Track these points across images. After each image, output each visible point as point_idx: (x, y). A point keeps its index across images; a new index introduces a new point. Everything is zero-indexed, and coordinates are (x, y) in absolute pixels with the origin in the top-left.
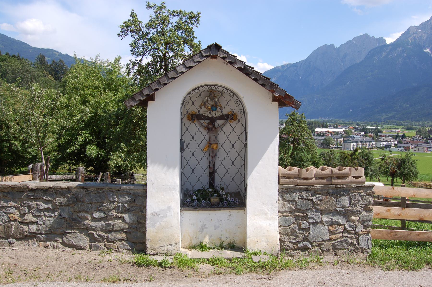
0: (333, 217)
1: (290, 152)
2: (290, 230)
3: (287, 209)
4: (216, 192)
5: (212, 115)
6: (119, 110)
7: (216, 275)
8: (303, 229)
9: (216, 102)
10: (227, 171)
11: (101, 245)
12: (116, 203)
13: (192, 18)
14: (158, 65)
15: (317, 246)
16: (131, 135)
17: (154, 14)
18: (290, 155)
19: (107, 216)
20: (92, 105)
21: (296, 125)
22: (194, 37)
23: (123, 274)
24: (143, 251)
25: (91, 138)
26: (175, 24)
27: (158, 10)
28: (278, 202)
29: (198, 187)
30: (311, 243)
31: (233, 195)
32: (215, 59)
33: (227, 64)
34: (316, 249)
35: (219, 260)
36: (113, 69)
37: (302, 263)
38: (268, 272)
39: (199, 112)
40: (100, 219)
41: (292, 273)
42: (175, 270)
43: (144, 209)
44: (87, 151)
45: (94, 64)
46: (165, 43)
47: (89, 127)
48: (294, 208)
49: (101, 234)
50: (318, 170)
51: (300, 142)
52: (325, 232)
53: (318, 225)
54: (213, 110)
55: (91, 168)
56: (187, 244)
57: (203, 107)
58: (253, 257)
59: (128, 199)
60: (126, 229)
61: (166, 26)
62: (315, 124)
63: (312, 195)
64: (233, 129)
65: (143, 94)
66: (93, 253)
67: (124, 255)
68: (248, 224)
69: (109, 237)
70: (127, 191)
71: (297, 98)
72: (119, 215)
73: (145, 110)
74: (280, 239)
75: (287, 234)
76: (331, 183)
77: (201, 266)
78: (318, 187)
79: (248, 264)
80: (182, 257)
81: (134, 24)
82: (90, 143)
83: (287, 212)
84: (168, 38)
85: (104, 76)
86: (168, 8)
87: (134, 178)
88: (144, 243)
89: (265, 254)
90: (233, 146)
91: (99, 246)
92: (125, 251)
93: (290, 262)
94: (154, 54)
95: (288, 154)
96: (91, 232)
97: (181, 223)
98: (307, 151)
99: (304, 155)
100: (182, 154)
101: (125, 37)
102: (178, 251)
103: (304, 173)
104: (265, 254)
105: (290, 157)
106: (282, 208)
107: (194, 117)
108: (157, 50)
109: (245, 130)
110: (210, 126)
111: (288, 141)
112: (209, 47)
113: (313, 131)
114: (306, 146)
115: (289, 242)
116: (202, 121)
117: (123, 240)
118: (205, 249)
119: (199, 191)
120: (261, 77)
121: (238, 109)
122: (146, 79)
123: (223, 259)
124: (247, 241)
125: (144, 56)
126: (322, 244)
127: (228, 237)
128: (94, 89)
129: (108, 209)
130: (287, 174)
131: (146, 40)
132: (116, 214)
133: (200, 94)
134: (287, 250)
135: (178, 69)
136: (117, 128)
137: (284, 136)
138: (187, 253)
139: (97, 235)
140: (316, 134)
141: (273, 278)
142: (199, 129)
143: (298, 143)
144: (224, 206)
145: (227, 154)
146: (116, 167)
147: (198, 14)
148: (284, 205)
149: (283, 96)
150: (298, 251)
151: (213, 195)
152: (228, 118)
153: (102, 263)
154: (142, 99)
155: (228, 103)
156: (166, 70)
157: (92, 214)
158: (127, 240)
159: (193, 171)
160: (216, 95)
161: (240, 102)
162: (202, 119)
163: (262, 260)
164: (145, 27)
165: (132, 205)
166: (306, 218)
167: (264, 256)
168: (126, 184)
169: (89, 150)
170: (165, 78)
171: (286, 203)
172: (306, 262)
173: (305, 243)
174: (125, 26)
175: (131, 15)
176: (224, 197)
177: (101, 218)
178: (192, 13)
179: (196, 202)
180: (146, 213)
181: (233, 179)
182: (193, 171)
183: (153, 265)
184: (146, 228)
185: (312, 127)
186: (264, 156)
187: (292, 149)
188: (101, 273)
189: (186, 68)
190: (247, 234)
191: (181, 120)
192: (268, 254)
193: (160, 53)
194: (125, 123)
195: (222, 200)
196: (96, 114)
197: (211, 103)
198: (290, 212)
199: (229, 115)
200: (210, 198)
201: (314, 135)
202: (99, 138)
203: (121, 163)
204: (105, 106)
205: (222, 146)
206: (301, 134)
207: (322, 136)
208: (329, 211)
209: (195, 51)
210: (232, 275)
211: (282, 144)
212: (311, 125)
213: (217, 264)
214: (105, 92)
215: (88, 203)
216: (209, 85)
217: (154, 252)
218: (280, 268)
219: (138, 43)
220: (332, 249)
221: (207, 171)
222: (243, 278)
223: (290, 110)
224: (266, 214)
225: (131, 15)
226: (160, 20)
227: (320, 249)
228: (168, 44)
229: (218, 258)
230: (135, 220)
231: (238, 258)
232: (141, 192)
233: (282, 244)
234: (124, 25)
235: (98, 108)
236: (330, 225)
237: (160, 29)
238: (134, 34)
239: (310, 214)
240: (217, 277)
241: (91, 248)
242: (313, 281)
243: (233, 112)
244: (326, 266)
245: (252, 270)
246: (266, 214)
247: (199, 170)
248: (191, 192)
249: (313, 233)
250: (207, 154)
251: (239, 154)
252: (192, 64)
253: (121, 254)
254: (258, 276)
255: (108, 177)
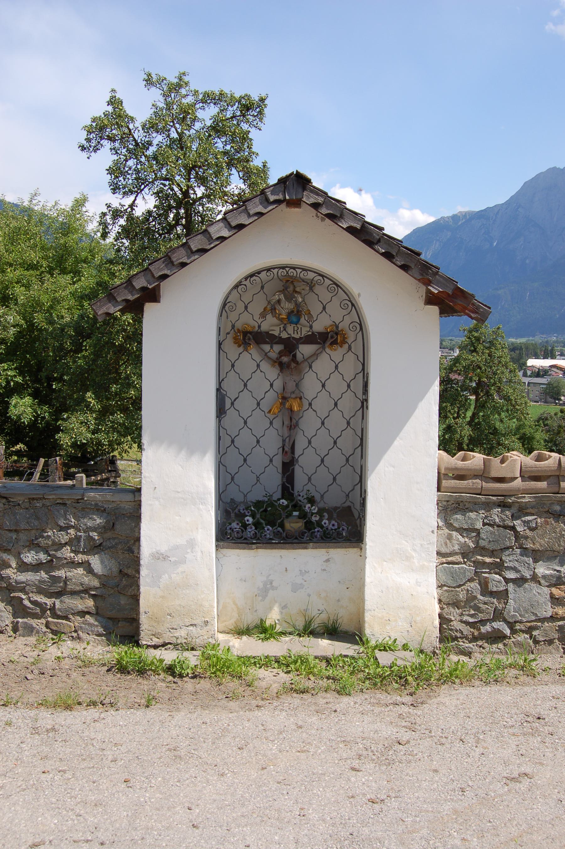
0: (562, 566)
1: (469, 414)
2: (462, 596)
3: (456, 548)
4: (296, 506)
5: (290, 337)
6: (82, 317)
7: (295, 695)
8: (492, 594)
9: (297, 305)
10: (322, 461)
11: (38, 624)
12: (72, 531)
13: (248, 109)
14: (172, 216)
15: (522, 631)
16: (110, 373)
17: (162, 99)
18: (468, 419)
19: (52, 560)
20: (23, 304)
21: (483, 353)
22: (251, 153)
23: (87, 692)
24: (132, 637)
25: (19, 379)
26: (209, 123)
27: (170, 91)
28: (436, 531)
29: (257, 495)
30: (511, 625)
31: (335, 515)
32: (295, 207)
33: (323, 220)
34: (522, 637)
35: (303, 660)
36: (69, 225)
37: (490, 670)
38: (413, 690)
39: (259, 327)
40: (36, 567)
41: (467, 692)
42: (202, 681)
43: (134, 543)
44: (12, 408)
45: (27, 212)
46: (185, 166)
47: (15, 355)
48: (472, 545)
49: (39, 600)
50: (528, 460)
51: (492, 392)
52: (542, 600)
53: (526, 585)
54: (291, 323)
55: (20, 446)
56: (230, 623)
57: (269, 317)
58: (378, 654)
59: (99, 521)
60: (96, 588)
61: (190, 127)
62: (527, 348)
63: (514, 517)
64: (337, 367)
65: (133, 287)
66: (21, 641)
67: (89, 647)
68: (368, 580)
69: (57, 606)
70: (96, 505)
71: (480, 296)
72: (80, 558)
73: (139, 320)
74: (440, 616)
75: (456, 604)
76: (556, 490)
77: (262, 673)
78: (527, 499)
79: (367, 671)
80: (220, 654)
81: (117, 123)
82: (18, 390)
83: (456, 554)
84: (192, 155)
85: (48, 240)
86: (192, 87)
87: (116, 470)
88: (134, 621)
89: (405, 647)
90: (336, 404)
91: (35, 625)
92: (91, 638)
93: (463, 667)
94: (161, 191)
95: (464, 418)
96: (16, 594)
97: (218, 576)
98: (507, 410)
99: (501, 421)
100: (220, 421)
101: (95, 152)
102: (210, 640)
103: (497, 468)
104: (405, 647)
105: (469, 423)
106: (446, 544)
107: (249, 338)
108: (167, 183)
109: (363, 369)
110: (285, 359)
111: (465, 388)
112: (283, 181)
113: (523, 366)
114: (505, 399)
115: (461, 621)
116: (267, 347)
117: (89, 613)
118: (271, 634)
119: (258, 504)
120: (399, 250)
121: (347, 320)
122: (144, 248)
123: (311, 659)
124: (366, 619)
125: (140, 196)
126: (536, 628)
127: (322, 608)
128: (27, 269)
129: (54, 543)
130: (456, 469)
131: (143, 159)
132: (72, 555)
133: (262, 287)
134: (455, 639)
135: (212, 230)
136: (79, 358)
137: (456, 376)
138: (231, 644)
139: (31, 602)
140: (529, 373)
141: (422, 703)
142: (258, 366)
143: (488, 394)
144: (315, 540)
145: (323, 423)
146: (74, 445)
147: (262, 100)
148: (450, 537)
149: (450, 293)
150: (480, 643)
151: (289, 515)
152: (324, 342)
153: (40, 665)
154: (130, 297)
155: (324, 308)
156: (189, 227)
157: (18, 556)
158: (97, 614)
159: (245, 460)
160: (298, 289)
161: (353, 305)
162: (266, 343)
163: (400, 662)
164: (140, 129)
165: (109, 534)
166: (499, 568)
167: (402, 654)
168: (100, 483)
169: (15, 406)
170: (182, 251)
171: (454, 533)
172: (498, 668)
173: (496, 625)
174: (96, 128)
175: (110, 103)
176: (315, 519)
177: (38, 565)
178: (248, 97)
179: (251, 530)
180: (139, 553)
181: (334, 479)
182: (245, 460)
183: (154, 671)
184: (138, 586)
185: (520, 357)
186: (406, 428)
187: (472, 407)
188: (37, 687)
189: (230, 227)
190: (366, 603)
191: (220, 344)
192: (411, 648)
193: (176, 189)
194: (95, 346)
195: (309, 525)
196: (31, 326)
197: (288, 306)
198: (464, 555)
199: (327, 333)
200: (283, 521)
201: (525, 375)
202: (37, 380)
203: (85, 436)
204: (51, 307)
205: (310, 404)
206: (495, 374)
207: (542, 376)
208: (551, 553)
209: (253, 183)
210: (331, 696)
211: (449, 397)
212: (517, 352)
213: (297, 670)
214: (52, 275)
215: (10, 531)
216: (283, 268)
217: (156, 641)
218: (439, 680)
219: (125, 165)
220: (559, 639)
221: (278, 462)
222: (355, 703)
223: (465, 322)
224: (408, 558)
225: (110, 103)
226: (175, 113)
227: (531, 637)
228: (194, 167)
229: (300, 657)
230: (115, 570)
231: (346, 656)
232: (128, 507)
233: (445, 626)
234: (94, 124)
235: (36, 312)
236: (555, 585)
237: (174, 135)
238: (117, 144)
239: (509, 559)
240: (296, 700)
241: (15, 629)
242: (513, 712)
243: (337, 327)
244: (545, 677)
245: (375, 684)
246: (408, 558)
247: (259, 459)
248: (241, 508)
249: (515, 602)
250: (277, 423)
251: (348, 423)
252: (244, 220)
253: (84, 645)
254: (389, 699)
255: (57, 469)
